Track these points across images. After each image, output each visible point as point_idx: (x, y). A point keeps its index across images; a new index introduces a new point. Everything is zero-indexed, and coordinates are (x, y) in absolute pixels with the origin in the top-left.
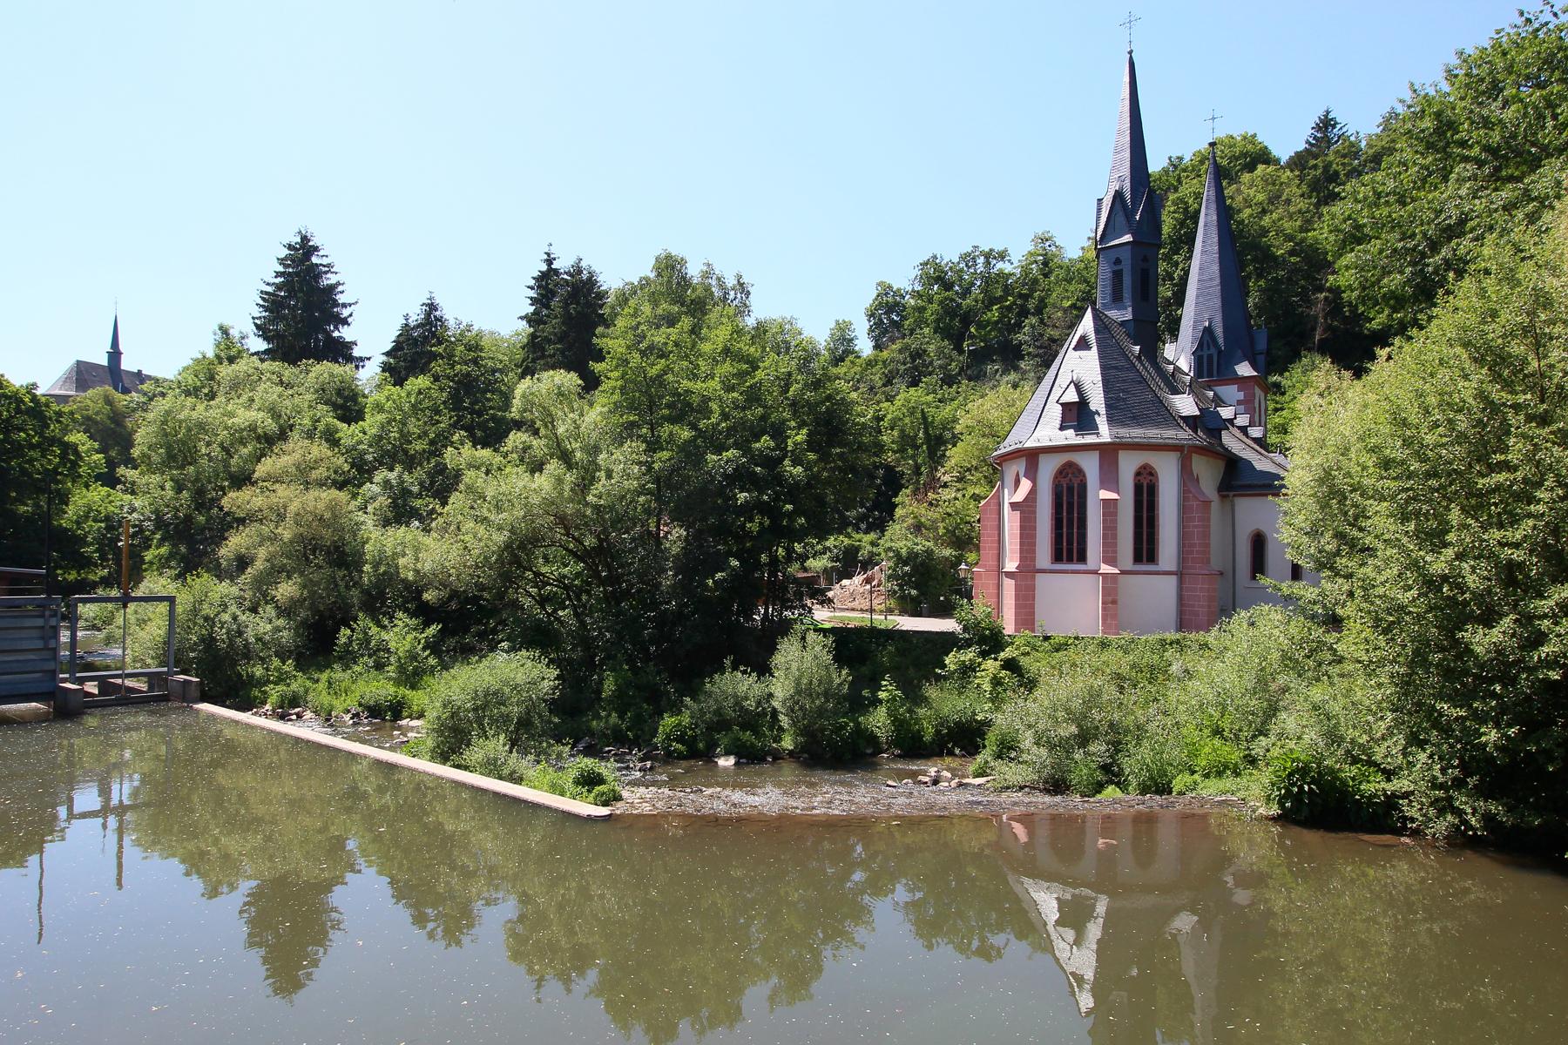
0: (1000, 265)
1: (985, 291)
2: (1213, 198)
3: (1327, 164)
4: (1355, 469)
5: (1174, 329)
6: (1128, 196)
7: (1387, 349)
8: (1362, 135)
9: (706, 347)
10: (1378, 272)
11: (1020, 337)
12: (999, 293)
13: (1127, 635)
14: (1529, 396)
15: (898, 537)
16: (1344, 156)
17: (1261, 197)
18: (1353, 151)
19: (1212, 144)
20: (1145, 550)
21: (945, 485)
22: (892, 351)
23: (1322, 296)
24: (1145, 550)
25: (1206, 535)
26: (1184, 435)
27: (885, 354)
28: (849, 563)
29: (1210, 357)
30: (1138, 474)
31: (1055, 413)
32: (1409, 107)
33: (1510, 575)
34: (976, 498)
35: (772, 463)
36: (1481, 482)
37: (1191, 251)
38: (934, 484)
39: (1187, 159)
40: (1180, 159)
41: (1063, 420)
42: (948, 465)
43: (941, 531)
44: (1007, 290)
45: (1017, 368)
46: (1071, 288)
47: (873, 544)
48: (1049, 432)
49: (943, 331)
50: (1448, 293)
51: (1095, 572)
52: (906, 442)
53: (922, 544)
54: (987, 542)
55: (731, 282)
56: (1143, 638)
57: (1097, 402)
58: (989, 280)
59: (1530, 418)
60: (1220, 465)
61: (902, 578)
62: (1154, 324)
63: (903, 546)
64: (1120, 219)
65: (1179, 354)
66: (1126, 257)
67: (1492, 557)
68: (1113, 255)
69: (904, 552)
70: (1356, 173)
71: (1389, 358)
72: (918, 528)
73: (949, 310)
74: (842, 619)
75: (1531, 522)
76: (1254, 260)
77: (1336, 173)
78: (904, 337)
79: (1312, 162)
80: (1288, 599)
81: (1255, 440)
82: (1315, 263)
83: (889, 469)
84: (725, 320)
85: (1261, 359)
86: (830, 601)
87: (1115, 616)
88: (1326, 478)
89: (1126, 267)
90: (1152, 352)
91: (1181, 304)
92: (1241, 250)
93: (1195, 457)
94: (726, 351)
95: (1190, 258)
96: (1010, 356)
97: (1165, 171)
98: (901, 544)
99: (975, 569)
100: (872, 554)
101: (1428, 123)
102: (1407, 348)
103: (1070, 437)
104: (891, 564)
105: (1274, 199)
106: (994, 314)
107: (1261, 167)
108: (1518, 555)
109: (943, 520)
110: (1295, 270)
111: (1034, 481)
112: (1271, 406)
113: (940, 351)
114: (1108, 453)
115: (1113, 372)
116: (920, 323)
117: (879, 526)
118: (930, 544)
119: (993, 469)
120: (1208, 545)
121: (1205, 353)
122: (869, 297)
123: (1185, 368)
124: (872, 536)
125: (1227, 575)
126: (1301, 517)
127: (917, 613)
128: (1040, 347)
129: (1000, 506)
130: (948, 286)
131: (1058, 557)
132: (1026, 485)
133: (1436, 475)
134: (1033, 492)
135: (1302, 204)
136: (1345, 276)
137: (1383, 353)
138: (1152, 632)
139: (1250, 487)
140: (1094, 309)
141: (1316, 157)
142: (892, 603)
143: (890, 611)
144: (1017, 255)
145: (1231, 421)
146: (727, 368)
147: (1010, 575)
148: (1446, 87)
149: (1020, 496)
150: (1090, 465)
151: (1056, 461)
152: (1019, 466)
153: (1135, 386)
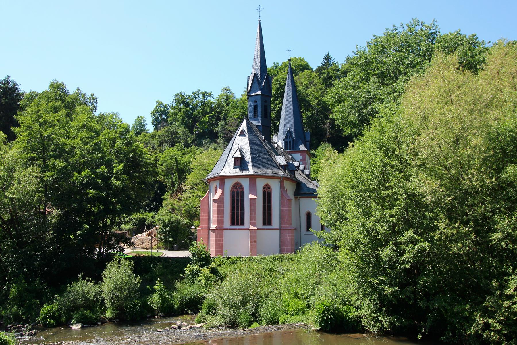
0: (209, 98)
1: (203, 109)
3: (328, 73)
5: (277, 131)
6: (259, 76)
10: (347, 114)
12: (208, 110)
13: (261, 256)
15: (164, 214)
16: (334, 70)
17: (306, 82)
19: (290, 60)
20: (267, 220)
21: (185, 191)
23: (328, 121)
24: (267, 220)
25: (290, 213)
26: (281, 172)
27: (159, 132)
28: (141, 226)
29: (290, 142)
30: (264, 188)
34: (199, 197)
38: (180, 190)
39: (280, 64)
40: (278, 64)
41: (235, 164)
42: (188, 181)
43: (183, 211)
44: (212, 109)
45: (215, 142)
46: (238, 111)
47: (152, 217)
49: (186, 125)
51: (248, 229)
52: (169, 172)
53: (175, 217)
54: (203, 216)
57: (248, 158)
58: (205, 104)
61: (166, 233)
62: (269, 127)
64: (256, 85)
65: (278, 140)
66: (259, 99)
68: (254, 99)
69: (167, 221)
71: (353, 146)
72: (173, 210)
73: (188, 116)
77: (332, 76)
78: (168, 125)
79: (323, 71)
82: (325, 109)
83: (161, 183)
85: (308, 143)
87: (255, 248)
88: (333, 191)
89: (259, 104)
90: (268, 139)
92: (300, 102)
94: (84, 126)
95: (282, 102)
96: (213, 136)
97: (273, 68)
98: (166, 217)
100: (152, 222)
101: (362, 61)
103: (237, 172)
104: (161, 226)
105: (311, 83)
106: (206, 118)
110: (318, 111)
112: (312, 162)
113: (184, 133)
114: (253, 178)
116: (174, 120)
117: (155, 209)
119: (207, 184)
121: (288, 140)
122: (153, 106)
124: (152, 214)
125: (297, 229)
128: (225, 134)
130: (187, 105)
131: (233, 223)
132: (219, 192)
134: (222, 195)
135: (320, 86)
138: (270, 254)
139: (305, 194)
140: (247, 120)
141: (325, 69)
142: (161, 244)
143: (160, 248)
144: (216, 94)
145: (298, 167)
147: (213, 231)
148: (367, 49)
149: (217, 197)
150: (245, 184)
151: (235, 180)
153: (262, 152)
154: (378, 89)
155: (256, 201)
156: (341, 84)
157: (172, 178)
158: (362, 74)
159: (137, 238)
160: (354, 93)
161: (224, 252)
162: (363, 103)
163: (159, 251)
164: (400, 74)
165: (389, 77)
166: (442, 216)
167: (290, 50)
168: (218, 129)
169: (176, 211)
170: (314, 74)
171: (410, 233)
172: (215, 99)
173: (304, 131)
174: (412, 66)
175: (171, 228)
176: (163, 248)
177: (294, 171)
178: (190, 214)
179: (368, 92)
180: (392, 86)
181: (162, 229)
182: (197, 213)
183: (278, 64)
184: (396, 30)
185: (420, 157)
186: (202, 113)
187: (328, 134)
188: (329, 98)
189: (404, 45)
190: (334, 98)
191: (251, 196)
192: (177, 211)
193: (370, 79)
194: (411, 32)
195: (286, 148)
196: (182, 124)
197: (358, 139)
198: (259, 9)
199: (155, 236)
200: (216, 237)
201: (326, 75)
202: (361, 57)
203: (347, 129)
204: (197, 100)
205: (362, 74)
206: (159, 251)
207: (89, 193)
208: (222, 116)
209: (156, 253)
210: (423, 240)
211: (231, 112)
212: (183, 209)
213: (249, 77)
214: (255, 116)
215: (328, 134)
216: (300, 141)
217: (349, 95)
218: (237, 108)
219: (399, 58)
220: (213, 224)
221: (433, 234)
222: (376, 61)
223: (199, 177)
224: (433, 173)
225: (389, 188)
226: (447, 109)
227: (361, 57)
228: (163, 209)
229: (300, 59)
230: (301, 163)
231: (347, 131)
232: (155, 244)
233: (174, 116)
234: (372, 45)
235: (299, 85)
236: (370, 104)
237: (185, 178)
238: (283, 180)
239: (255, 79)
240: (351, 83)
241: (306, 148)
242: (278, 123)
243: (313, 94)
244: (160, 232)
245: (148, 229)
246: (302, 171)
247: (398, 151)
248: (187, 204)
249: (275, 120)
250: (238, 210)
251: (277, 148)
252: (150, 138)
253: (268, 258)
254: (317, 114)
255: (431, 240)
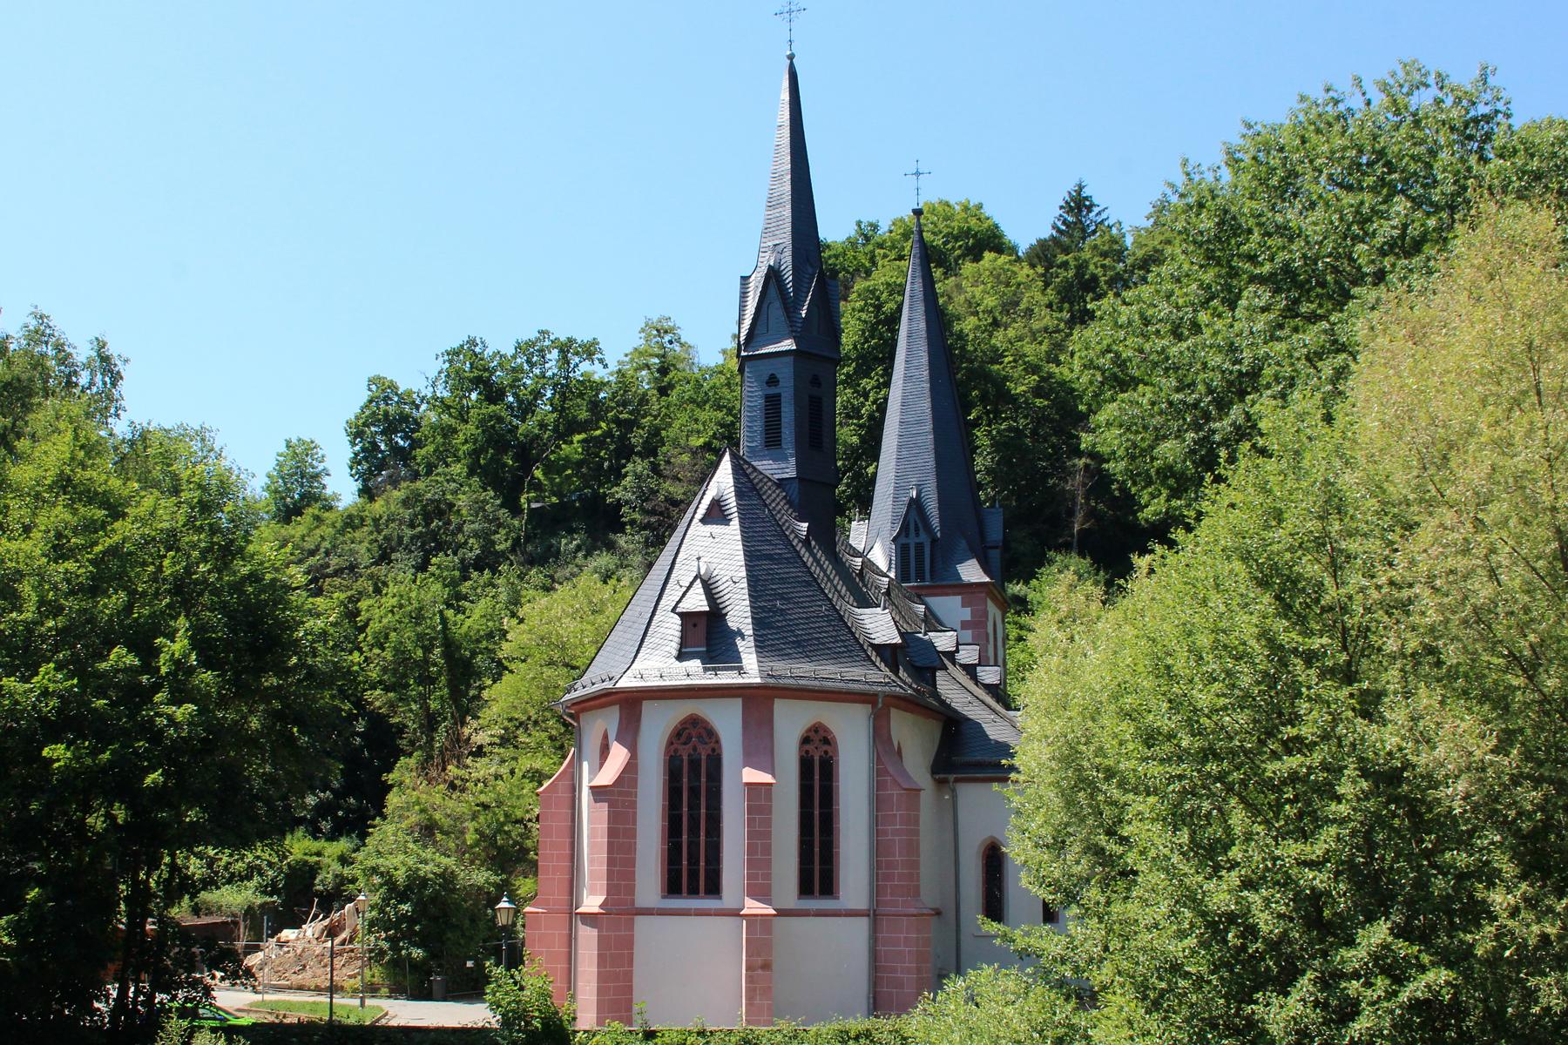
0: (585, 366)
1: (560, 409)
2: (920, 296)
3: (1081, 264)
4: (1110, 745)
5: (864, 502)
6: (788, 277)
7: (1148, 558)
8: (1126, 228)
9: (21, 474)
10: (1149, 436)
11: (619, 493)
12: (584, 415)
13: (786, 1026)
14: (1325, 640)
15: (391, 848)
16: (1104, 255)
17: (990, 302)
18: (1115, 251)
19: (918, 213)
20: (818, 875)
21: (479, 752)
22: (389, 502)
23: (1081, 462)
24: (818, 875)
25: (912, 848)
26: (876, 676)
27: (378, 507)
28: (298, 897)
29: (920, 547)
30: (805, 740)
31: (669, 628)
32: (1182, 196)
33: (1311, 907)
34: (537, 777)
35: (135, 695)
36: (1272, 768)
37: (888, 372)
38: (459, 749)
39: (884, 228)
40: (875, 227)
41: (684, 642)
42: (487, 714)
43: (470, 838)
44: (596, 407)
45: (611, 547)
46: (703, 415)
47: (344, 860)
48: (659, 663)
49: (491, 476)
50: (1218, 479)
51: (735, 913)
52: (399, 677)
53: (434, 862)
54: (549, 856)
55: (82, 352)
56: (813, 1029)
57: (739, 615)
58: (566, 391)
59: (1325, 673)
60: (934, 730)
61: (396, 925)
62: (829, 487)
63: (399, 865)
64: (776, 311)
65: (872, 541)
66: (785, 372)
67: (1287, 882)
68: (766, 369)
69: (400, 876)
70: (1120, 282)
71: (1152, 571)
72: (428, 830)
73: (496, 438)
74: (273, 1008)
75: (1333, 830)
76: (984, 399)
77: (1095, 278)
78: (415, 476)
79: (1061, 258)
80: (1025, 956)
81: (989, 688)
82: (1066, 413)
83: (378, 722)
84: (62, 425)
85: (995, 555)
86: (249, 973)
87: (767, 991)
88: (1070, 757)
89: (786, 390)
90: (828, 536)
91: (874, 454)
92: (962, 381)
93: (894, 713)
94: (64, 483)
95: (887, 384)
96: (599, 523)
97: (852, 243)
98: (396, 860)
99: (532, 909)
100: (342, 880)
101: (1207, 223)
102: (1171, 559)
103: (693, 672)
104: (375, 899)
105: (1010, 305)
106: (573, 448)
107: (988, 256)
108: (1318, 879)
109: (474, 817)
110: (1040, 419)
111: (633, 749)
112: (1014, 633)
113: (479, 507)
114: (757, 700)
115: (766, 565)
116: (444, 455)
117: (356, 825)
118: (449, 862)
119: (566, 726)
120: (915, 865)
121: (912, 541)
122: (353, 400)
123: (882, 564)
124: (343, 845)
125: (946, 915)
126: (1039, 819)
127: (422, 993)
128: (653, 512)
129: (574, 790)
130: (493, 394)
131: (673, 887)
132: (619, 755)
133: (1218, 757)
134: (631, 768)
135: (1044, 319)
136: (1107, 432)
137: (1141, 562)
138: (825, 1018)
139: (980, 766)
140: (734, 456)
141: (1066, 251)
142: (376, 974)
143: (372, 990)
144: (616, 350)
145: (951, 656)
146: (59, 514)
147: (589, 919)
148: (1227, 175)
149: (607, 776)
150: (727, 722)
151: (680, 711)
152: (606, 722)
153: (796, 590)
154: (1273, 338)
155: (769, 797)
156: (1125, 313)
157: (423, 698)
158: (1208, 276)
159: (281, 944)
160: (1174, 351)
161: (636, 1008)
162: (1210, 391)
163: (368, 1002)
164: (1358, 280)
165: (1315, 289)
166: (1509, 869)
167: (918, 174)
168: (622, 492)
169: (439, 837)
170: (1024, 272)
171: (1377, 934)
172: (613, 367)
173: (978, 503)
174: (1407, 246)
175: (421, 908)
176: (384, 991)
177: (933, 671)
178: (499, 849)
179: (1232, 349)
180: (1325, 325)
181: (381, 911)
182: (529, 843)
183: (875, 227)
184: (1336, 102)
185: (1415, 619)
186: (556, 430)
187: (1079, 516)
188: (1077, 368)
189: (1370, 164)
190: (1098, 368)
191: (752, 775)
192: (447, 834)
193: (1239, 296)
194: (1397, 113)
195: (904, 574)
196: (471, 473)
197: (1172, 544)
198: (789, 13)
199: (351, 940)
200: (602, 942)
201: (1071, 273)
202: (1201, 206)
203: (1153, 497)
204: (537, 371)
205: (1208, 276)
206: (368, 1002)
207: (51, 761)
208: (637, 438)
209: (352, 1009)
210: (1426, 959)
211: (676, 424)
212: (471, 825)
213: (745, 280)
214: (772, 441)
215: (1079, 516)
216: (963, 544)
217: (1154, 357)
218: (701, 405)
219: (1346, 217)
220: (593, 892)
221: (1469, 938)
222: (1260, 225)
223: (537, 695)
224: (1468, 685)
225: (1294, 745)
226: (1518, 426)
227: (1201, 206)
228: (389, 828)
229: (966, 209)
230: (968, 635)
231: (1153, 507)
232: (346, 973)
233: (439, 439)
234: (1247, 158)
235: (962, 310)
236: (1242, 394)
237: (478, 697)
238: (887, 706)
239: (773, 291)
240: (1164, 309)
241: (987, 571)
242: (870, 470)
243: (1018, 347)
244: (372, 924)
245: (326, 909)
246: (970, 670)
247: (1331, 595)
248: (485, 807)
249: (859, 458)
250: (694, 830)
251: (861, 574)
252: (342, 532)
253: (818, 1035)
254: (1034, 432)
255: (1457, 958)
